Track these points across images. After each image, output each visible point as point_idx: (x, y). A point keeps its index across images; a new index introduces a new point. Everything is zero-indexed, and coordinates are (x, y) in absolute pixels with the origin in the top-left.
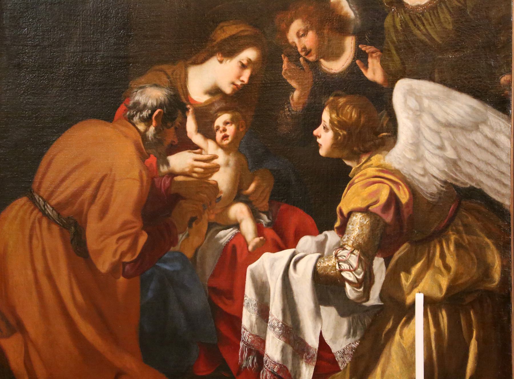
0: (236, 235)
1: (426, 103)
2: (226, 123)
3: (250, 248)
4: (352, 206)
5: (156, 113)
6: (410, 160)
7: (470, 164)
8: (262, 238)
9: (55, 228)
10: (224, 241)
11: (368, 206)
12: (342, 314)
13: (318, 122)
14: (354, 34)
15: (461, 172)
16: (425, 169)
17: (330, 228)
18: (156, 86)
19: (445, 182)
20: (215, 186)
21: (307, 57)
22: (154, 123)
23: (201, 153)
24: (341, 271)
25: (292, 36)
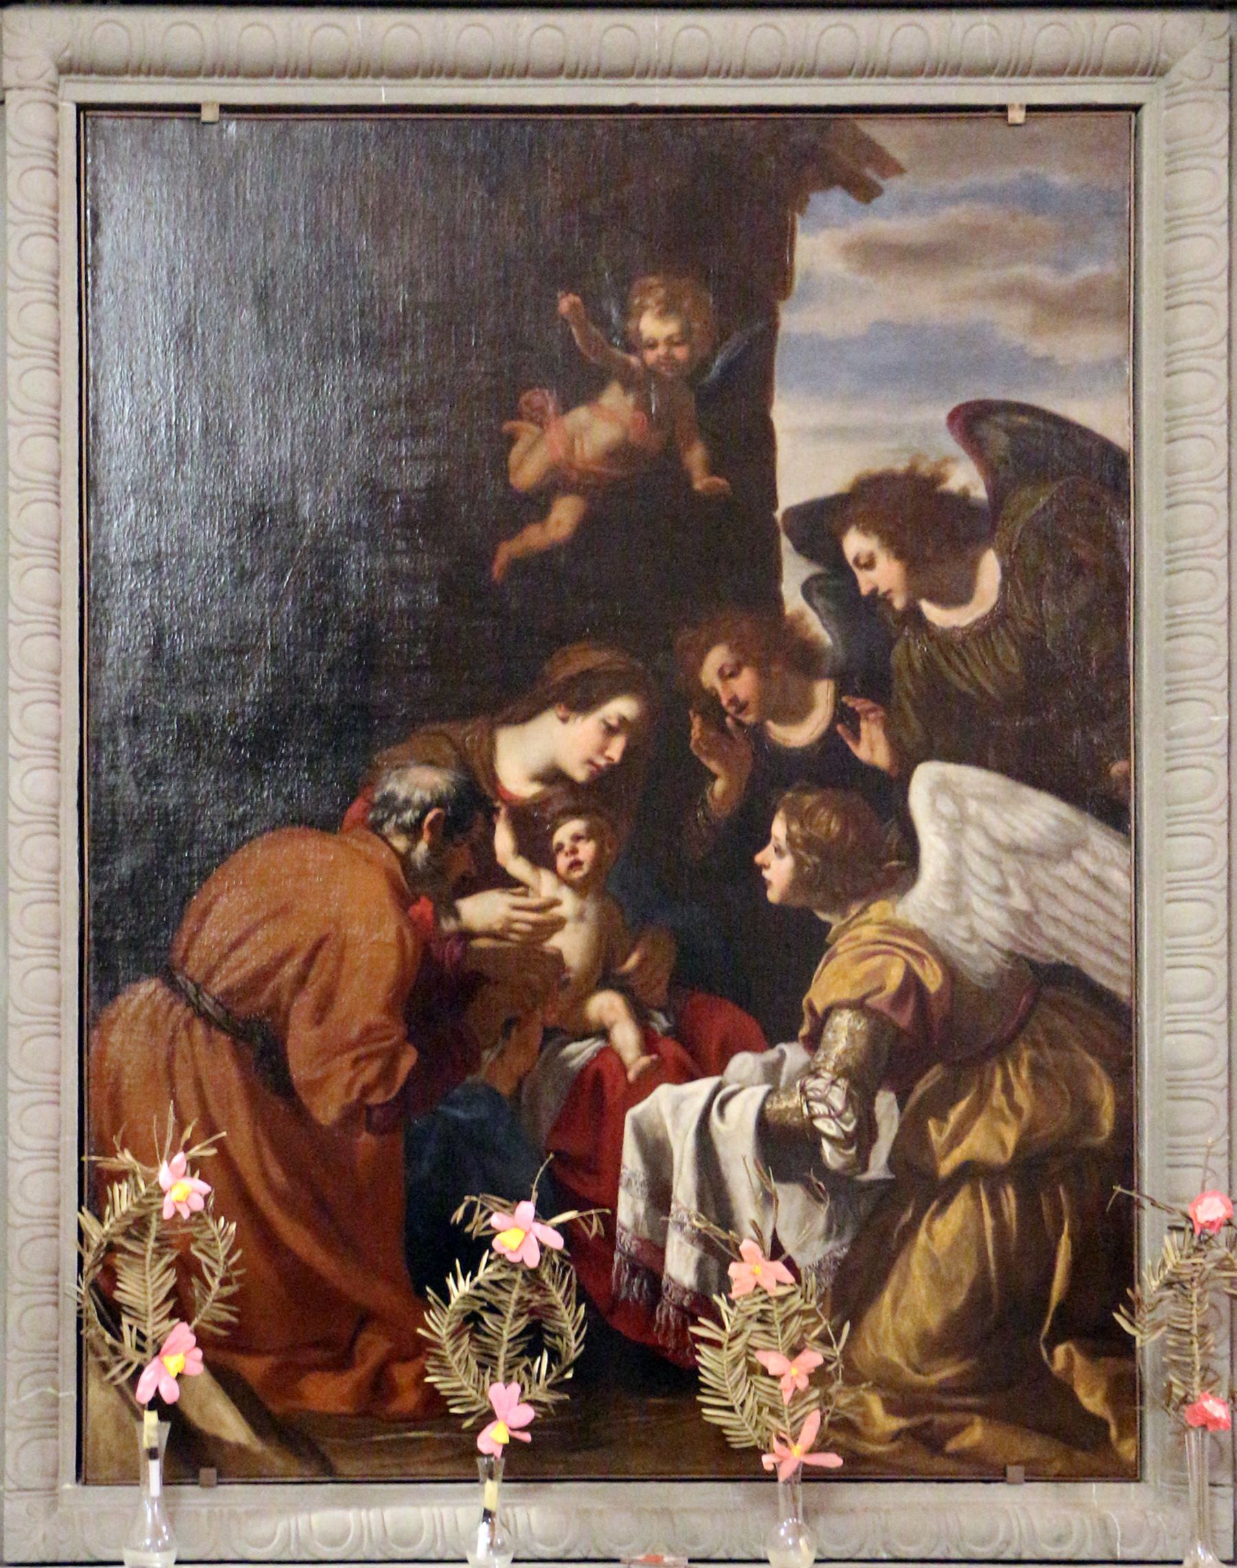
0: (601, 1052)
1: (973, 807)
2: (577, 838)
3: (631, 1076)
4: (833, 997)
5: (430, 816)
6: (943, 912)
7: (1056, 920)
8: (654, 1057)
10: (576, 1063)
12: (815, 1195)
13: (764, 839)
15: (1040, 934)
16: (972, 930)
17: (791, 1037)
18: (431, 763)
19: (1011, 954)
20: (558, 958)
21: (740, 717)
22: (426, 836)
23: (525, 895)
24: (813, 1117)
25: (709, 674)
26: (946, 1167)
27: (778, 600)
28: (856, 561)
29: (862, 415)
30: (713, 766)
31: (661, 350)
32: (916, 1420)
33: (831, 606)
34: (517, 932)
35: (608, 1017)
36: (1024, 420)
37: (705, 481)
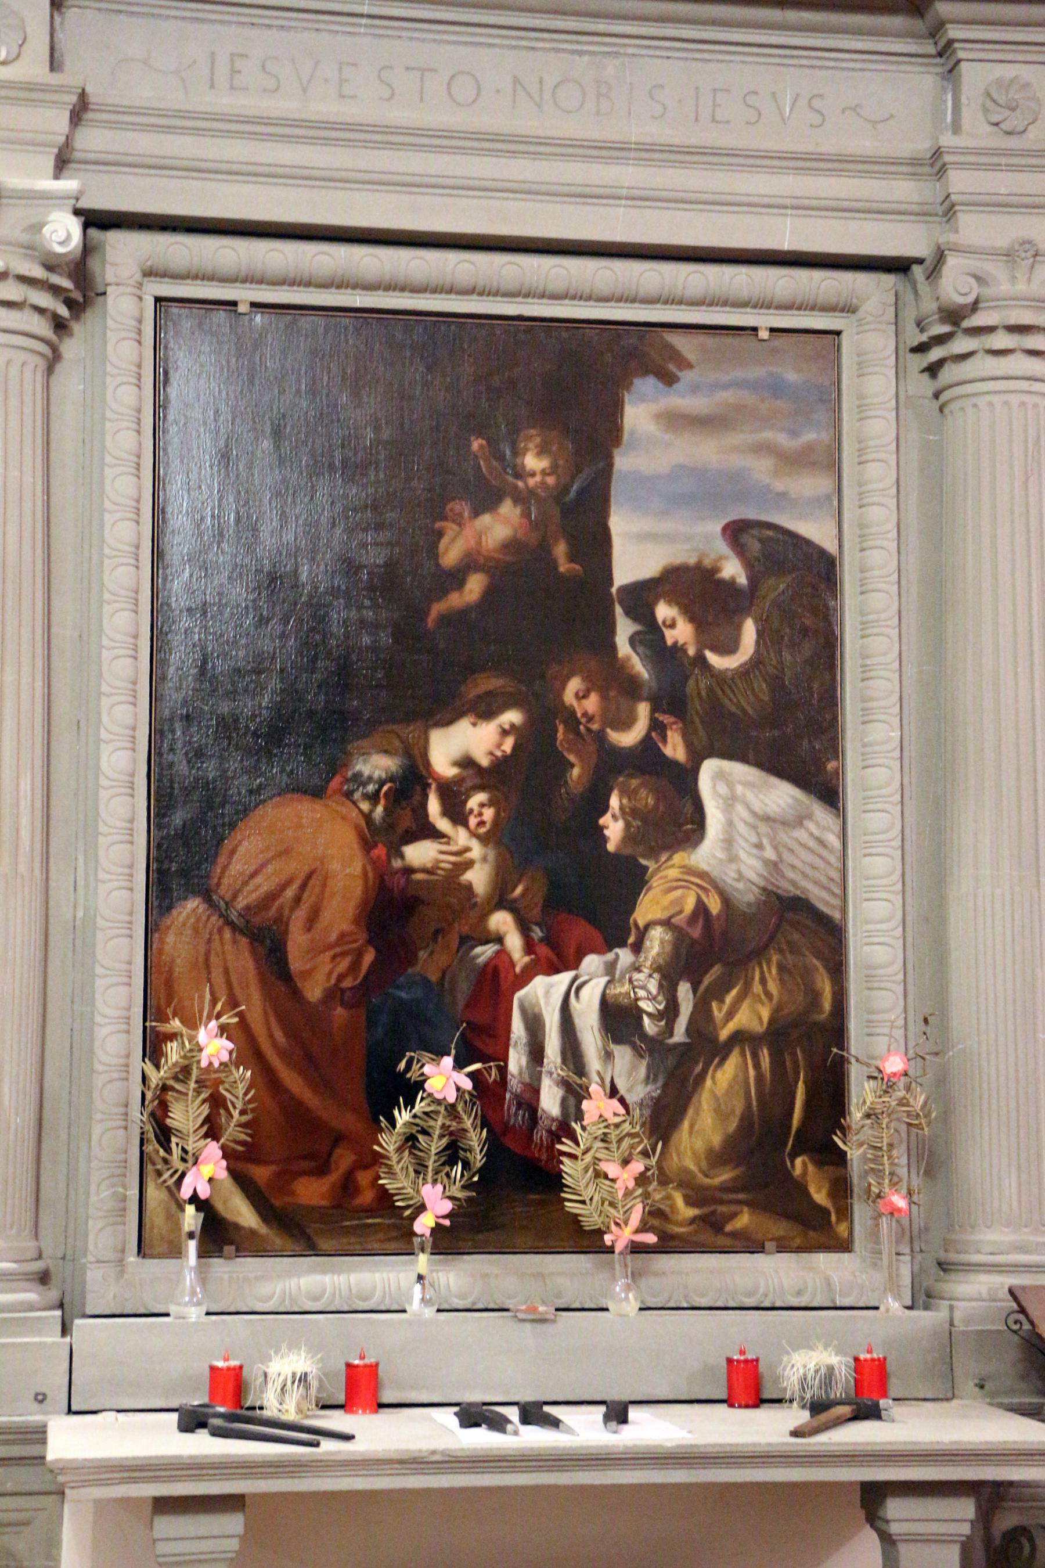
0: (498, 953)
1: (739, 789)
2: (482, 805)
3: (518, 969)
4: (650, 917)
5: (385, 788)
7: (793, 867)
8: (533, 956)
9: (244, 941)
10: (481, 960)
11: (671, 917)
12: (639, 1054)
13: (605, 808)
14: (647, 699)
15: (783, 876)
17: (622, 944)
18: (386, 752)
20: (469, 887)
21: (589, 725)
22: (382, 801)
23: (448, 843)
24: (637, 999)
25: (569, 696)
26: (724, 1034)
27: (613, 647)
28: (664, 622)
29: (667, 526)
30: (572, 758)
31: (538, 478)
32: (706, 1210)
33: (648, 653)
34: (442, 869)
35: (503, 929)
36: (770, 533)
37: (567, 566)
